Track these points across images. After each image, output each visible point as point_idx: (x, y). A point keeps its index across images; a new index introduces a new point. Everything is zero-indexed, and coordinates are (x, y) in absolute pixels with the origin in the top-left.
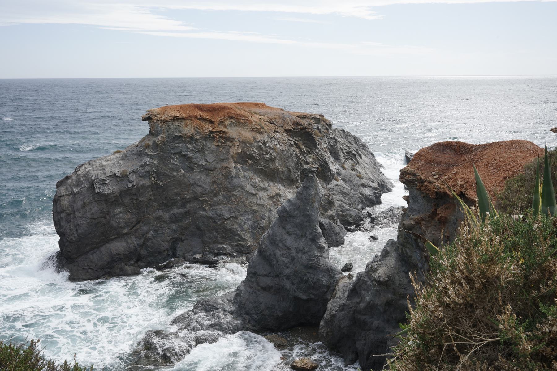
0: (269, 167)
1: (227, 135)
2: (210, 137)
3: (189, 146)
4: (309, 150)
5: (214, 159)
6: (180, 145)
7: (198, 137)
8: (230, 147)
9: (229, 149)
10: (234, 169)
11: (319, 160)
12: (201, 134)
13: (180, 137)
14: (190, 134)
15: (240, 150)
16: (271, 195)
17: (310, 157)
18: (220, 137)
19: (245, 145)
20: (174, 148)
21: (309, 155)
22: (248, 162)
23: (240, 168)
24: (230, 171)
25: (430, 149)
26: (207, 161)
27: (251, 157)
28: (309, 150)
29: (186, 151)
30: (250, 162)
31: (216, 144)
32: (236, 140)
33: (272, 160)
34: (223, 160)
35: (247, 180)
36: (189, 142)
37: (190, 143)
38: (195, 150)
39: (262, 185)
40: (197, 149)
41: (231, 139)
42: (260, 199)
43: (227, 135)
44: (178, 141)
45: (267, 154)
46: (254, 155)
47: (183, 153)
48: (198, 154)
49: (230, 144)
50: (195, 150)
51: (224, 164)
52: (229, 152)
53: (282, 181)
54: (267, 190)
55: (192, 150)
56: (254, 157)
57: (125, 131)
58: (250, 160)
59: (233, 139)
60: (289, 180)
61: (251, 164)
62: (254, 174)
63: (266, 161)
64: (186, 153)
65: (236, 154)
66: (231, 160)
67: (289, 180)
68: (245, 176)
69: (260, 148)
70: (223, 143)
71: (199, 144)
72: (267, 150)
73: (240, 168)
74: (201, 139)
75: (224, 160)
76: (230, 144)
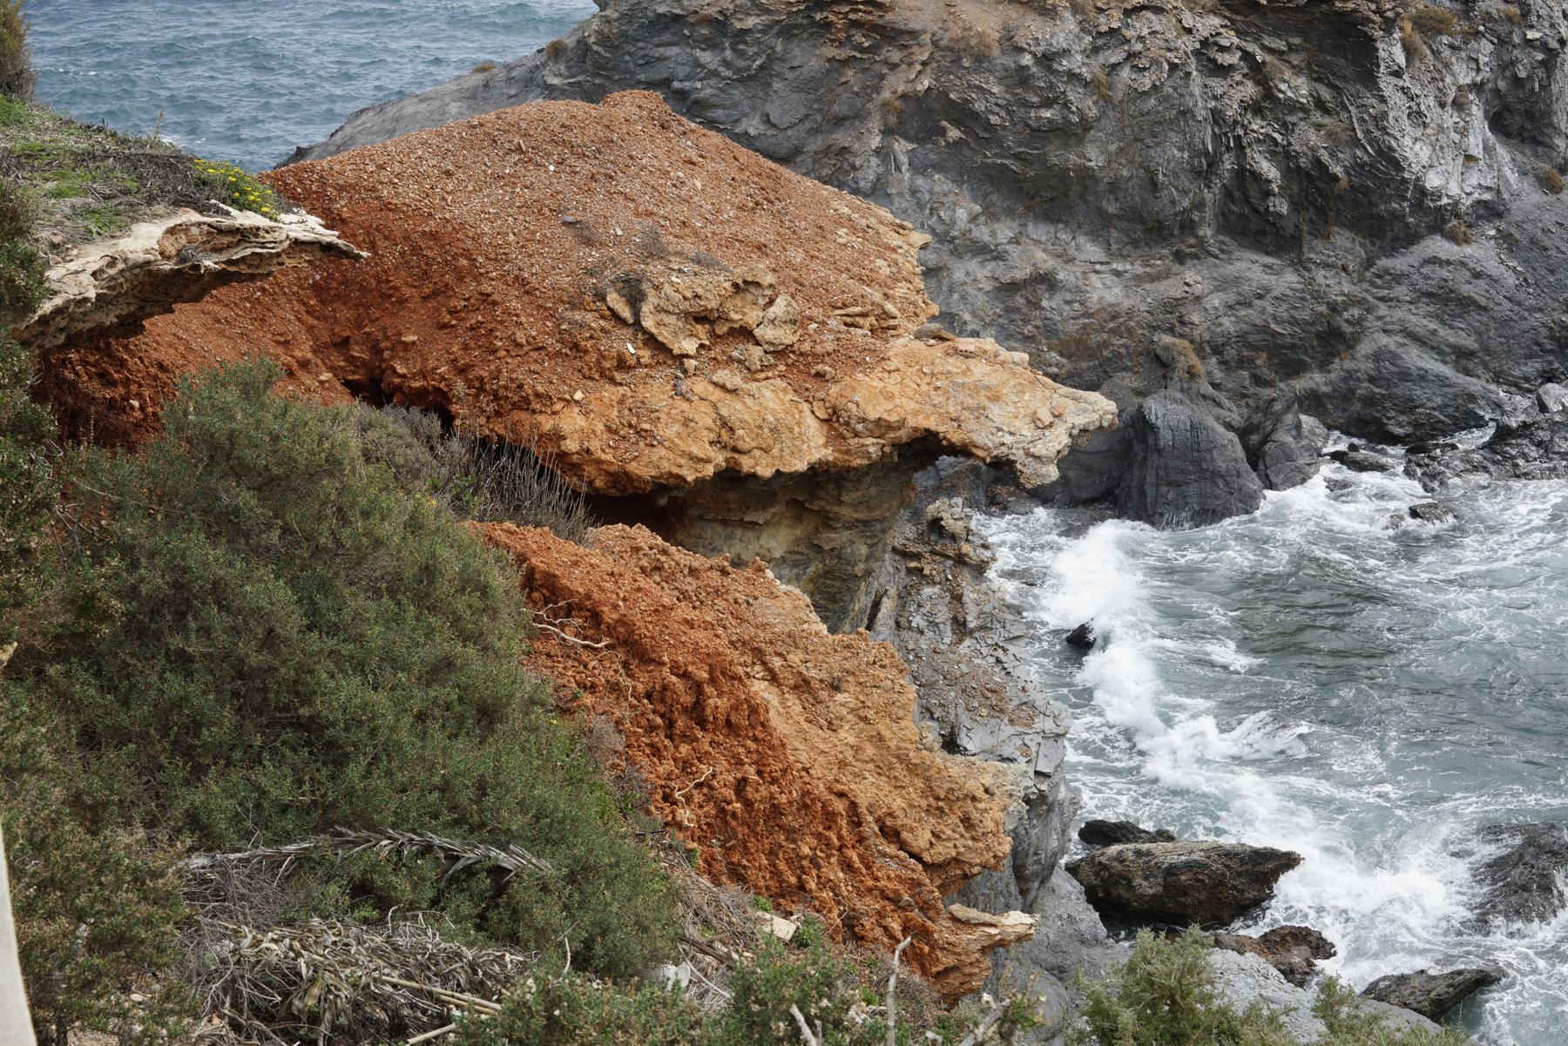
0: (1042, 159)
1: (890, 16)
2: (814, 23)
3: (706, 57)
4: (1326, 94)
5: (803, 111)
6: (673, 51)
7: (751, 22)
8: (893, 67)
9: (882, 77)
10: (874, 161)
11: (1356, 142)
12: (767, 11)
13: (676, 18)
14: (712, 11)
15: (926, 83)
16: (1006, 279)
17: (1319, 127)
18: (856, 24)
19: (957, 61)
20: (649, 63)
21: (1317, 117)
22: (943, 132)
23: (904, 159)
24: (854, 168)
25: (19, 880)
26: (767, 120)
27: (963, 115)
28: (1326, 94)
29: (687, 78)
30: (954, 133)
31: (831, 51)
32: (926, 38)
33: (1072, 132)
34: (839, 121)
35: (920, 206)
36: (706, 39)
37: (710, 44)
38: (728, 73)
39: (982, 233)
40: (739, 70)
41: (902, 32)
42: (951, 291)
43: (890, 16)
44: (667, 37)
45: (1047, 103)
46: (979, 106)
47: (676, 84)
48: (737, 93)
49: (895, 56)
50: (728, 73)
51: (842, 138)
52: (877, 89)
53: (1100, 226)
54: (1000, 257)
55: (715, 74)
56: (975, 116)
57: (1552, 26)
58: (957, 123)
59: (913, 34)
60: (1142, 220)
61: (958, 143)
62: (959, 184)
63: (1041, 133)
64: (687, 85)
65: (904, 97)
66: (875, 124)
67: (1142, 220)
68: (914, 192)
69: (1021, 77)
70: (864, 50)
71: (751, 51)
72: (1051, 87)
73: (904, 159)
74: (766, 29)
75: (845, 118)
76: (895, 56)
